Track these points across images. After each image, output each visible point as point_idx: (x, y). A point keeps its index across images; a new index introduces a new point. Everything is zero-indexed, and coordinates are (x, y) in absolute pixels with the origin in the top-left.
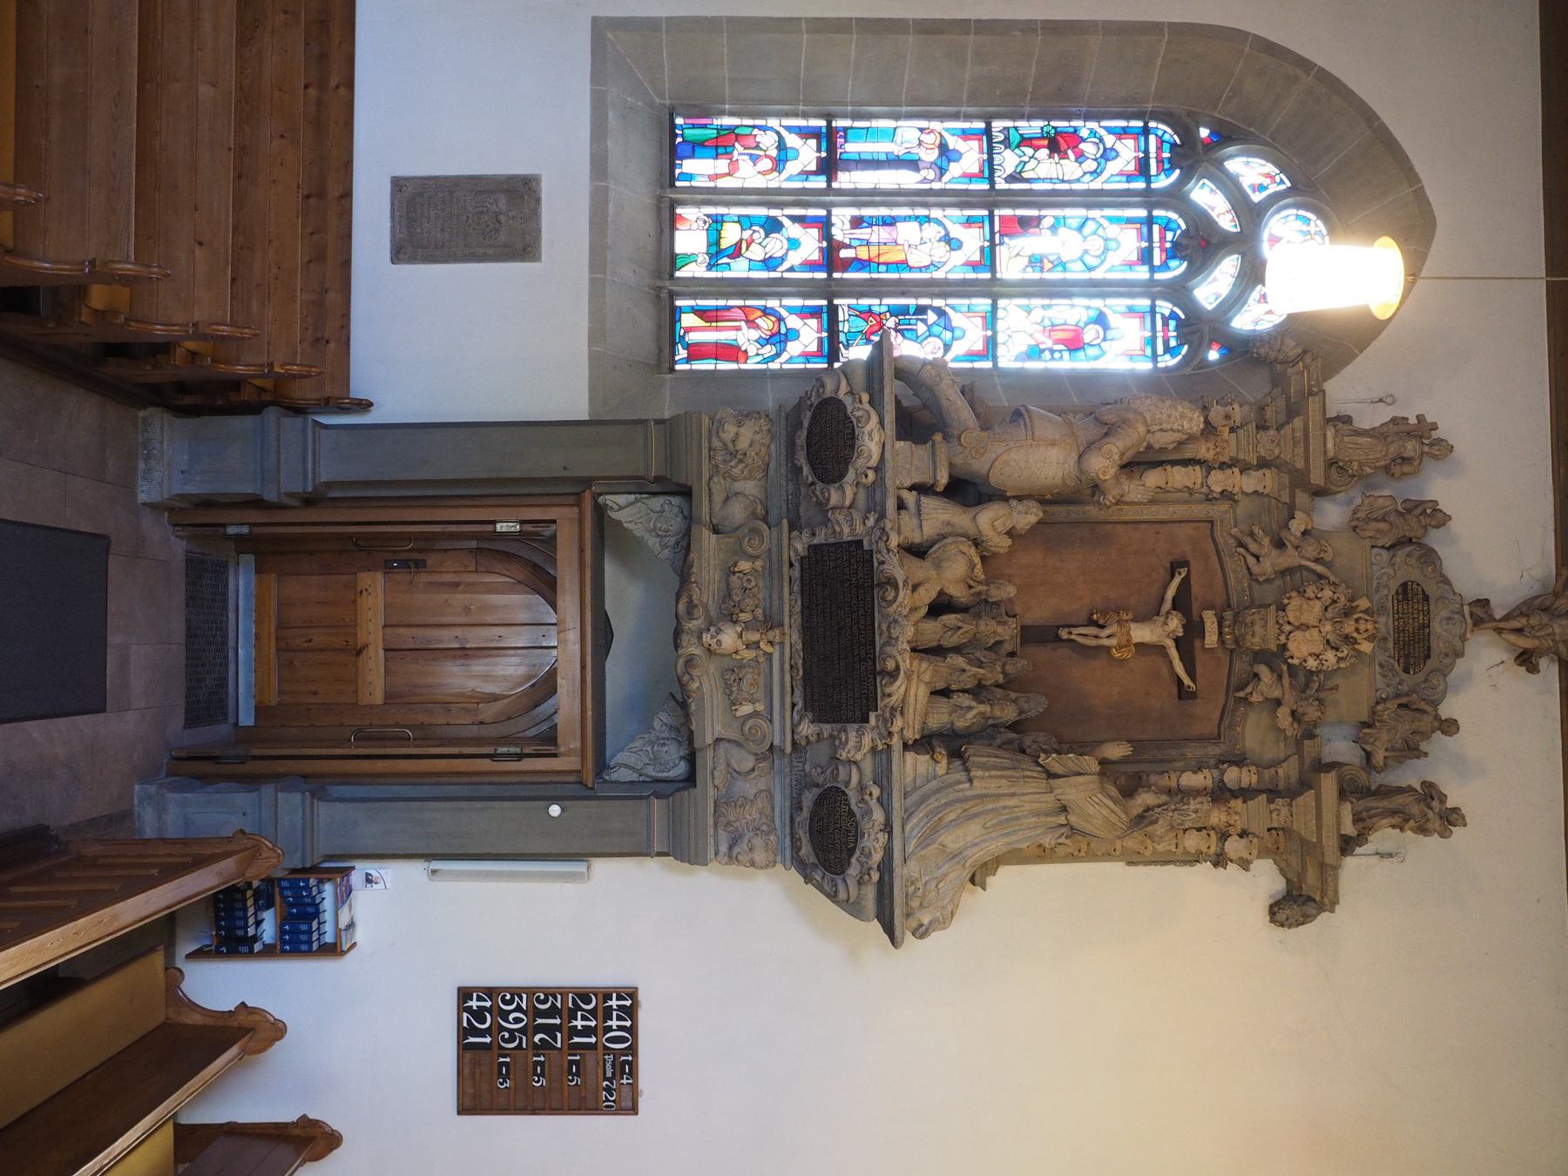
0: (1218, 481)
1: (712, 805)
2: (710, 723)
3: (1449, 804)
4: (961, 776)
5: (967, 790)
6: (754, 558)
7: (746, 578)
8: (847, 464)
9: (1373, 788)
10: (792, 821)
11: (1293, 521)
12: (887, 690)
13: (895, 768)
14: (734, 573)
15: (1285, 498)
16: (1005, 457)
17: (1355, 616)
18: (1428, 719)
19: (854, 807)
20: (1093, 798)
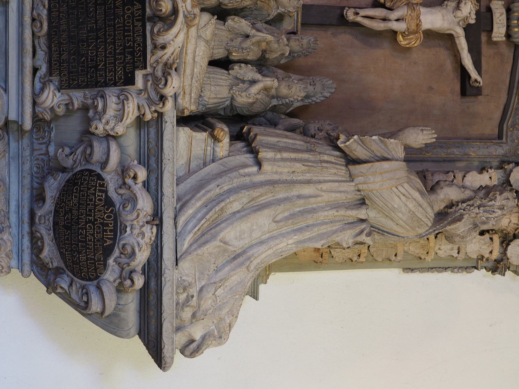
4: (248, 158)
5: (254, 174)
10: (32, 215)
12: (161, 40)
13: (166, 144)
19: (112, 193)
20: (400, 188)
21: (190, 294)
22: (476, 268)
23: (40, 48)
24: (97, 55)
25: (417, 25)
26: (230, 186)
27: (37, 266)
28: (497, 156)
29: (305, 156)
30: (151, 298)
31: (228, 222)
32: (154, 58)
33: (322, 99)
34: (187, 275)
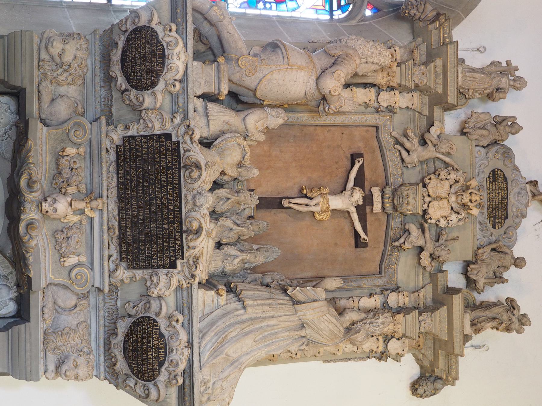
0: (386, 99)
1: (42, 334)
2: (44, 272)
3: (522, 312)
4: (238, 305)
5: (243, 315)
6: (78, 145)
7: (72, 161)
8: (158, 76)
9: (478, 304)
11: (432, 127)
12: (192, 244)
14: (63, 156)
15: (426, 112)
16: (269, 77)
17: (470, 191)
18: (508, 258)
19: (163, 330)
20: (324, 317)
21: (208, 386)
22: (368, 357)
23: (113, 243)
24: (151, 250)
25: (327, 208)
26: (230, 323)
27: (109, 374)
28: (379, 286)
29: (270, 302)
30: (186, 390)
31: (229, 343)
32: (188, 254)
33: (273, 259)
34: (206, 375)
